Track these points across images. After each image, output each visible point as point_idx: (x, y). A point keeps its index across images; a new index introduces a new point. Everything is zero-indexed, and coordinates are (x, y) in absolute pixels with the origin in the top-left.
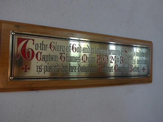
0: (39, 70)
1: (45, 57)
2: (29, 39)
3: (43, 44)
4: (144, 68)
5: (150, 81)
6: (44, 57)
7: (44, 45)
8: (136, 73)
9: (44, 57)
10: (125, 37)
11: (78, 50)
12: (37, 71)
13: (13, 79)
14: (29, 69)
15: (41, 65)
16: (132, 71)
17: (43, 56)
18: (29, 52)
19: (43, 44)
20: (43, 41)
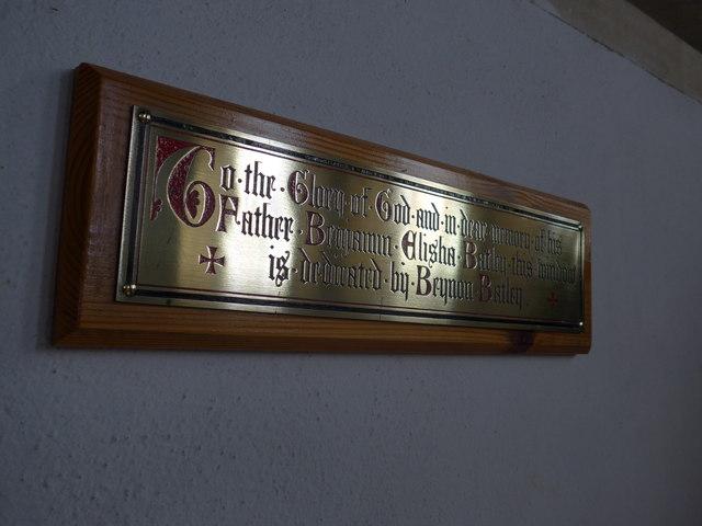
0: (276, 271)
1: (250, 218)
2: (201, 148)
3: (256, 171)
4: (553, 294)
5: (585, 349)
6: (247, 216)
7: (263, 177)
8: (416, 302)
9: (247, 216)
10: (144, 73)
11: (428, 219)
12: (273, 278)
13: (137, 292)
14: (222, 261)
15: (285, 256)
16: (397, 289)
17: (244, 216)
18: (196, 193)
19: (256, 171)
20: (256, 163)
